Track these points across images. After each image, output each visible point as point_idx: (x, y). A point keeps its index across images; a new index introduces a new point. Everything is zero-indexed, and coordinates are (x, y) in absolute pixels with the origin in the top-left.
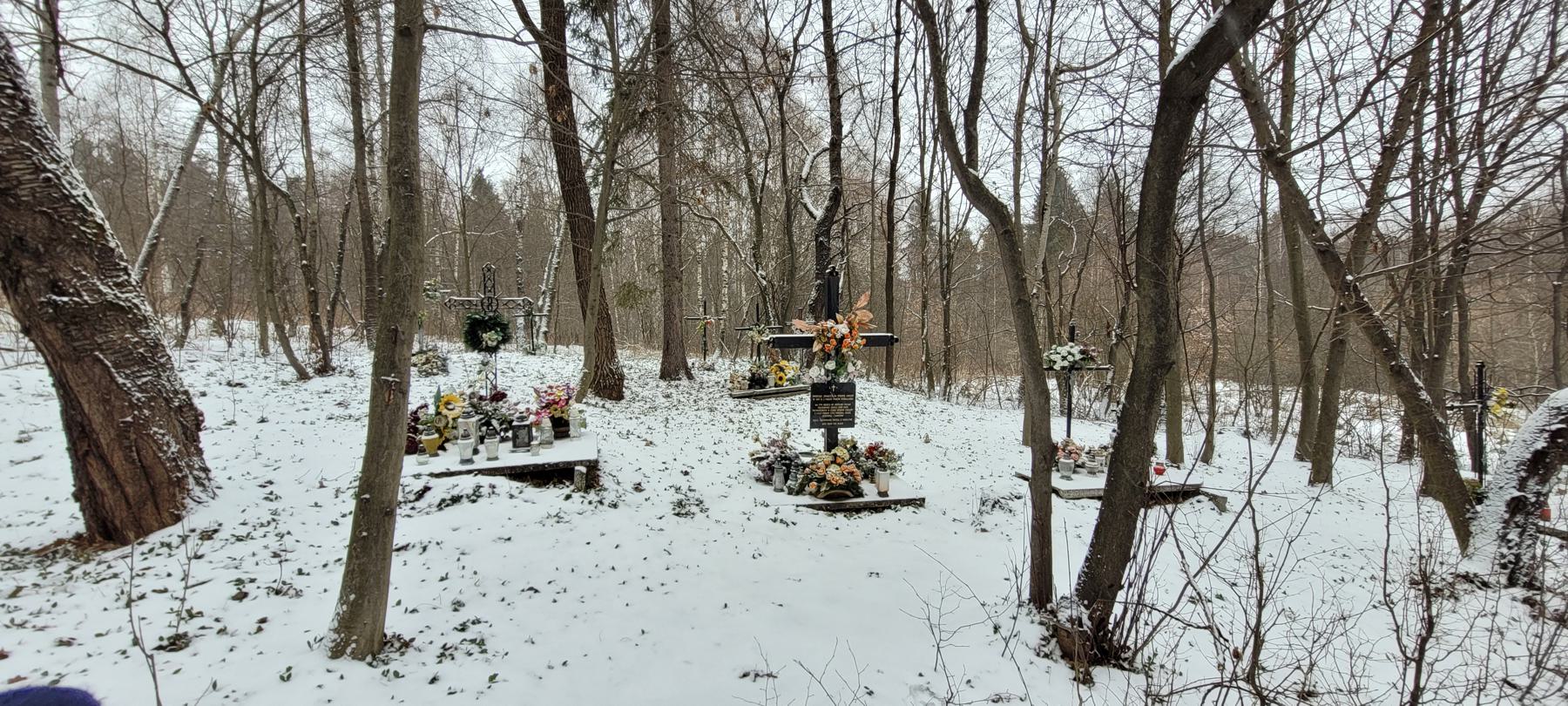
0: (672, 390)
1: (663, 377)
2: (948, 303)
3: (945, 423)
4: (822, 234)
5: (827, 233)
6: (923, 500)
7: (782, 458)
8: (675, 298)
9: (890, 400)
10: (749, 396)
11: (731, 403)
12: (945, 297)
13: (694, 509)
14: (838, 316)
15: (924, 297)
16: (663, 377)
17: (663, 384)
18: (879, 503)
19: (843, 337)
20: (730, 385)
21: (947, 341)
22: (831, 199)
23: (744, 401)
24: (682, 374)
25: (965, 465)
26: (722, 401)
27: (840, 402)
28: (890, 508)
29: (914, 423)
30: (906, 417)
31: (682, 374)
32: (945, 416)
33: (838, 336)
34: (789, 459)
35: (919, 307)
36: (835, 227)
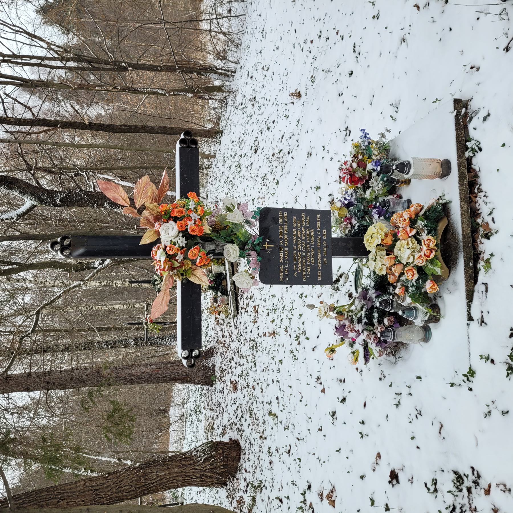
0: (227, 378)
1: (211, 384)
2: (130, 65)
3: (269, 73)
4: (52, 199)
5: (51, 193)
6: (457, 102)
7: (370, 323)
8: (124, 374)
9: (237, 134)
10: (236, 296)
11: (244, 318)
12: (125, 69)
13: (465, 490)
14: (146, 240)
15: (123, 90)
16: (211, 384)
17: (218, 385)
18: (461, 178)
19: (185, 233)
20: (223, 316)
21: (171, 69)
22: (10, 188)
23: (242, 303)
24: (209, 363)
25: (348, 43)
26: (241, 327)
27: (290, 234)
28: (469, 161)
29: (269, 110)
30: (260, 118)
31: (209, 363)
32: (258, 75)
33: (182, 242)
34: (371, 310)
35: (134, 98)
36: (44, 183)
